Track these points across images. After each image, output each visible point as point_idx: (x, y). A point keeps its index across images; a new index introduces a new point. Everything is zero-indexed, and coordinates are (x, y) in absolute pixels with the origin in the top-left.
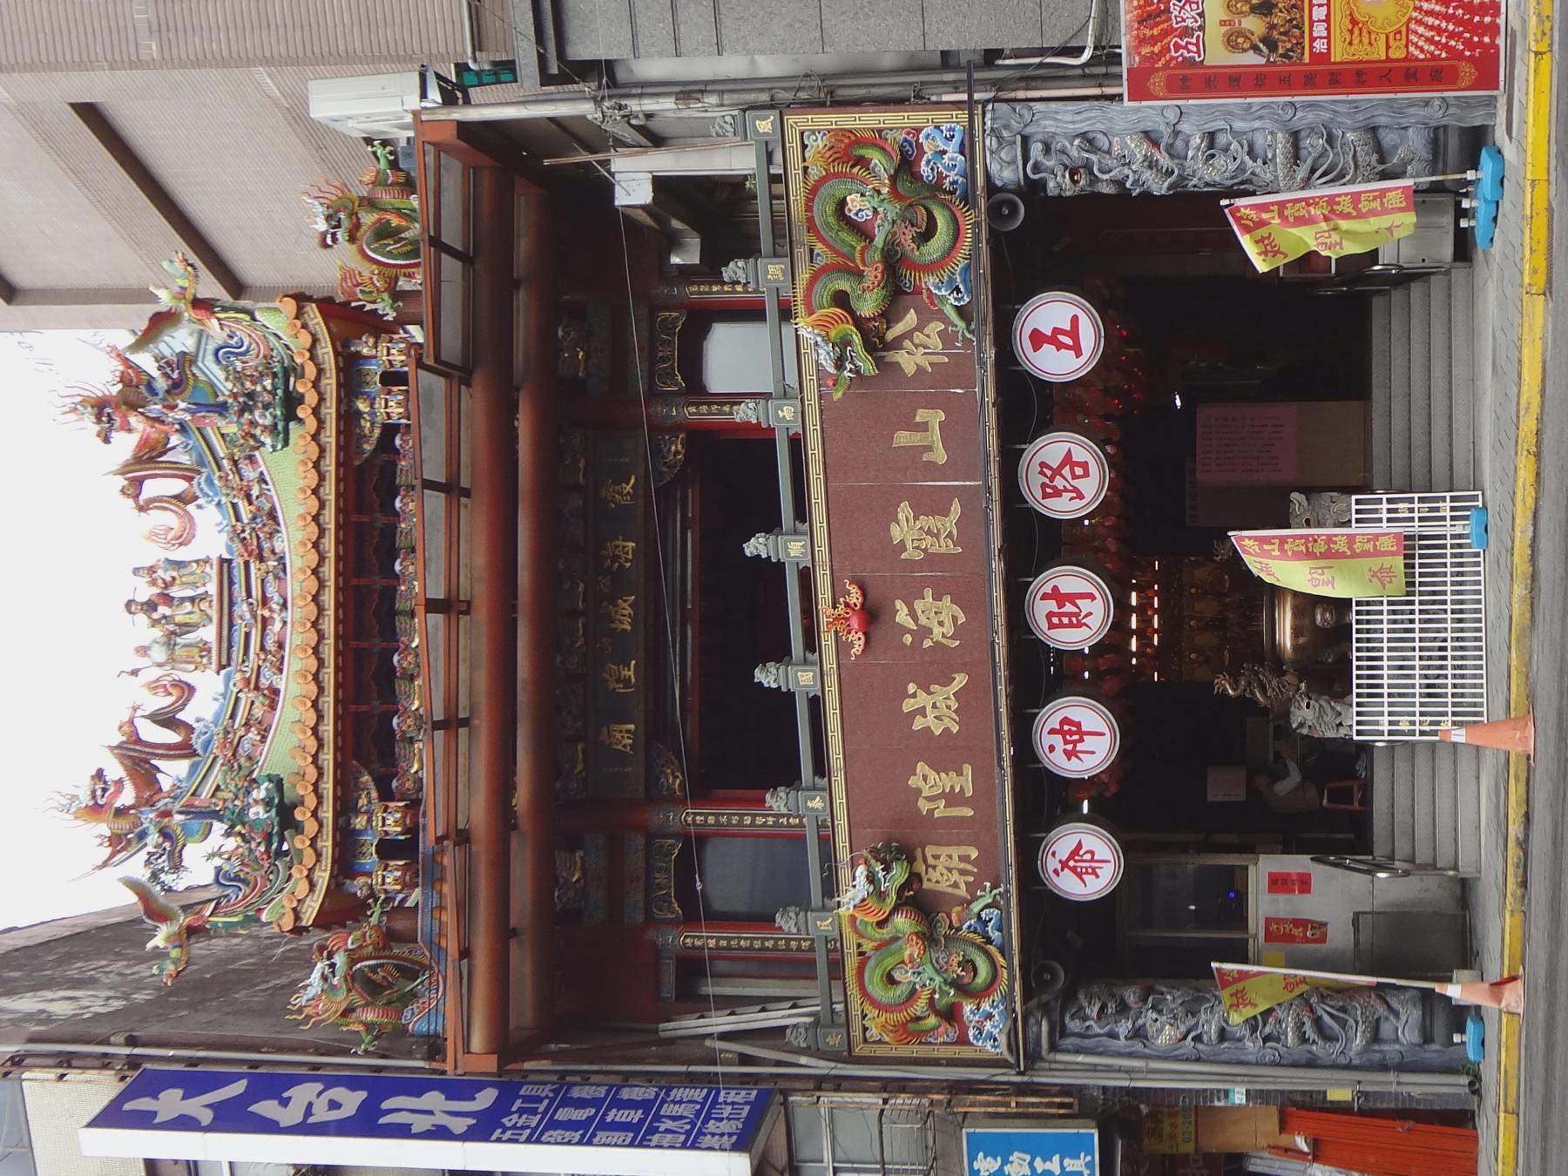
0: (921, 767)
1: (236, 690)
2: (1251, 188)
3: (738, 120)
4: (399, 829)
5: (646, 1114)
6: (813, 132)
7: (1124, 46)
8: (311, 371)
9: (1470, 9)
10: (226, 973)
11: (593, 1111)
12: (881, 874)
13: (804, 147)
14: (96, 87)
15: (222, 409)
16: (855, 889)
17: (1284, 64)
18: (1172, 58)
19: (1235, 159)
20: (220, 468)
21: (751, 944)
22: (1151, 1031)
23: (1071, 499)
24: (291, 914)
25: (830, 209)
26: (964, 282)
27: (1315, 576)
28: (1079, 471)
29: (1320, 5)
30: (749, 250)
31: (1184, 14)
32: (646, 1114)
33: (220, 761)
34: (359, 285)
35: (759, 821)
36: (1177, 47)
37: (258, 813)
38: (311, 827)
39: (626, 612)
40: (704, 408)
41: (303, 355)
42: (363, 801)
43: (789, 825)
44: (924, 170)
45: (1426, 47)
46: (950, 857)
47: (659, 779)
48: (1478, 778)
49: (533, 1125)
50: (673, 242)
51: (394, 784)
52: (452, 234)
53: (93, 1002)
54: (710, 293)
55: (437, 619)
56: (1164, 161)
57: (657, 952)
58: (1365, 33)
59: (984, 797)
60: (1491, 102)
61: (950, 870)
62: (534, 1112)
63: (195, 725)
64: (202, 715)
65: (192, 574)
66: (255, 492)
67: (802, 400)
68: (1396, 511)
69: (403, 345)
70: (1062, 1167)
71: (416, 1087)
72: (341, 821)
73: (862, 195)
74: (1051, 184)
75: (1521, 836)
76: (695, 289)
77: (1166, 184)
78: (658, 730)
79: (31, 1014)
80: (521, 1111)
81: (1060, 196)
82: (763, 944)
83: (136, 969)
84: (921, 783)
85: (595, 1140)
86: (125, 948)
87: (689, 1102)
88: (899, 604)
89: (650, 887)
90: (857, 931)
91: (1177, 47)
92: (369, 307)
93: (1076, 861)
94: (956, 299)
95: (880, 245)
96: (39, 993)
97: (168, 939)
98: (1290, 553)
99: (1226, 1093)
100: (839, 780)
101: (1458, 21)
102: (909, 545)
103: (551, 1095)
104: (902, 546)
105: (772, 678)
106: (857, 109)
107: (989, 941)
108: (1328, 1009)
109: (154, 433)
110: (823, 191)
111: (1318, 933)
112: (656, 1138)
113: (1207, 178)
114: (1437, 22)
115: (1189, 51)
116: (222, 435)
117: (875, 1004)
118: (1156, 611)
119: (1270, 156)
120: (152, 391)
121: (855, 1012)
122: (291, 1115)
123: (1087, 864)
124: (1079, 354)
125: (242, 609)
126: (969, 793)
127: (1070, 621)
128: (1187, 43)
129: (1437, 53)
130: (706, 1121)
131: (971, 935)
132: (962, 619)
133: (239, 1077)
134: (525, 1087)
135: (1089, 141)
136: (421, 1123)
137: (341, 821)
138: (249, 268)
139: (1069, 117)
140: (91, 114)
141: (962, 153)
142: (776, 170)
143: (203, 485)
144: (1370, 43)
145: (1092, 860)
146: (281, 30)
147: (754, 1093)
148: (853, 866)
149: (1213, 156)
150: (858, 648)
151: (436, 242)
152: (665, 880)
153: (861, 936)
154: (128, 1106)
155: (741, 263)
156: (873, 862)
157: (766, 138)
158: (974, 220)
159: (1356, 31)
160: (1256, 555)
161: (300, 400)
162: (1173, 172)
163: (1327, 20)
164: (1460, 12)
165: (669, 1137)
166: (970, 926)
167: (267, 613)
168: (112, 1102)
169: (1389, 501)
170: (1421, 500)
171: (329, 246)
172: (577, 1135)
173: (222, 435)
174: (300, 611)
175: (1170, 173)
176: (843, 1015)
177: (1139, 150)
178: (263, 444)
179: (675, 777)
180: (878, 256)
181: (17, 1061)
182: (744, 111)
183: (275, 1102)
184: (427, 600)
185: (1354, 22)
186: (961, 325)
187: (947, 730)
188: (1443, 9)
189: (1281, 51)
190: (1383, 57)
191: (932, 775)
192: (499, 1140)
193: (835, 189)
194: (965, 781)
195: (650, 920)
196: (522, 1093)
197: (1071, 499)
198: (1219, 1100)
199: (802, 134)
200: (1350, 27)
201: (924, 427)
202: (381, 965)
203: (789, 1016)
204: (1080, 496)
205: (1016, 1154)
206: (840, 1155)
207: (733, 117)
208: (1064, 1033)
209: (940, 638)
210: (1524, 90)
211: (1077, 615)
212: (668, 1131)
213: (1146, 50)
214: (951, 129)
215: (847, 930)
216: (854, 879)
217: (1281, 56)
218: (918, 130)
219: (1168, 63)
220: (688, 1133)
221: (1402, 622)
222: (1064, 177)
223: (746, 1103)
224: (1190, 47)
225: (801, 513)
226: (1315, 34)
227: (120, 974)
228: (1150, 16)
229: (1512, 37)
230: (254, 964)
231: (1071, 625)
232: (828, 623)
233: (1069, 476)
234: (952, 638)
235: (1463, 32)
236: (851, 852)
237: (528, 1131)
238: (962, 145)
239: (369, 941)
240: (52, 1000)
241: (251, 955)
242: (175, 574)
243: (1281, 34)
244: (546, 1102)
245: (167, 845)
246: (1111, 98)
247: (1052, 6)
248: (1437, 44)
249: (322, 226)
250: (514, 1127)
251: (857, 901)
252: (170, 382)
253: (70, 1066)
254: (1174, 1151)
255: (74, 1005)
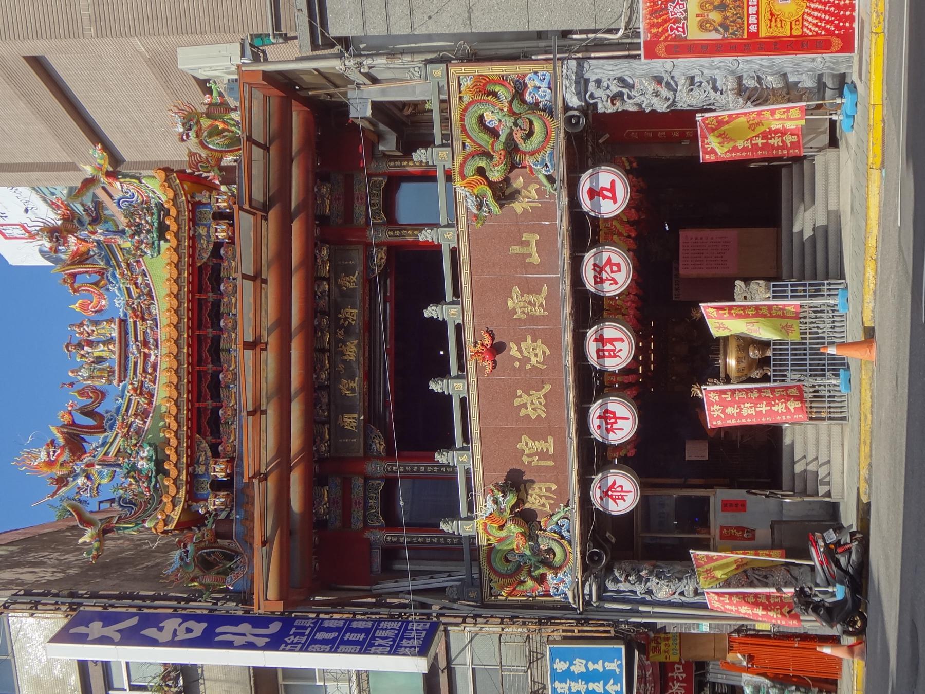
0: (524, 438)
1: (128, 395)
2: (714, 108)
3: (423, 69)
4: (223, 474)
5: (367, 636)
6: (465, 76)
7: (641, 27)
8: (173, 212)
9: (837, 7)
10: (118, 559)
11: (337, 634)
12: (501, 499)
13: (460, 85)
14: (37, 48)
15: (123, 233)
16: (485, 507)
17: (732, 39)
18: (669, 35)
19: (705, 92)
20: (120, 267)
21: (425, 540)
22: (654, 591)
23: (611, 284)
24: (162, 522)
25: (474, 120)
26: (551, 161)
27: (749, 327)
28: (615, 268)
29: (753, 6)
30: (428, 142)
31: (676, 11)
32: (367, 636)
33: (120, 436)
34: (200, 162)
35: (429, 469)
36: (672, 29)
37: (143, 465)
38: (174, 473)
39: (352, 350)
40: (397, 233)
41: (169, 203)
42: (202, 459)
43: (446, 472)
44: (528, 98)
45: (813, 29)
46: (540, 489)
47: (371, 445)
48: (843, 444)
49: (303, 642)
50: (380, 137)
51: (220, 448)
52: (258, 136)
53: (46, 574)
54: (401, 166)
55: (249, 353)
56: (664, 92)
57: (369, 544)
58: (778, 20)
59: (561, 454)
60: (850, 60)
61: (540, 496)
62: (303, 635)
63: (105, 415)
64: (109, 409)
65: (103, 328)
66: (140, 281)
67: (458, 228)
68: (796, 291)
69: (225, 197)
70: (604, 668)
71: (235, 621)
72: (190, 469)
73: (493, 112)
74: (600, 106)
75: (867, 476)
76: (392, 164)
77: (666, 106)
78: (373, 418)
79: (12, 581)
80: (295, 634)
81: (605, 113)
82: (431, 540)
83: (66, 556)
84: (524, 447)
85: (339, 650)
86: (58, 545)
87: (391, 629)
88: (512, 345)
89: (366, 508)
90: (487, 532)
91: (672, 29)
92: (205, 175)
93: (612, 492)
94: (546, 171)
95: (503, 141)
96: (14, 570)
97: (92, 537)
98: (734, 315)
99: (698, 625)
100: (477, 445)
101: (832, 14)
102: (518, 310)
103: (312, 625)
104: (514, 311)
105: (439, 387)
106: (490, 63)
107: (563, 538)
108: (757, 577)
109: (83, 248)
110: (470, 110)
111: (750, 535)
112: (373, 649)
113: (689, 102)
114: (819, 15)
115: (679, 31)
116: (121, 249)
117: (497, 573)
118: (653, 363)
119: (724, 90)
120: (81, 222)
121: (485, 579)
122: (166, 636)
123: (619, 494)
124: (615, 202)
125: (133, 349)
126: (552, 450)
127: (610, 354)
128: (678, 27)
129: (819, 32)
130: (401, 640)
131: (553, 534)
132: (548, 352)
133: (133, 615)
134: (297, 621)
135: (621, 80)
136: (238, 640)
137: (190, 469)
138: (127, 154)
139: (610, 68)
140: (39, 64)
141: (550, 88)
142: (445, 97)
143: (110, 278)
144: (781, 27)
145: (622, 491)
146: (164, 21)
147: (428, 624)
148: (485, 496)
149: (692, 90)
150: (488, 370)
151: (249, 139)
152: (375, 503)
153: (489, 534)
154: (72, 631)
155: (423, 151)
156: (496, 491)
157: (438, 80)
158: (558, 126)
159: (774, 20)
160: (716, 318)
161: (167, 228)
162: (669, 99)
163: (757, 14)
164: (832, 9)
165: (381, 648)
166: (552, 529)
167: (146, 351)
168: (63, 628)
169: (792, 286)
170: (810, 285)
171: (184, 141)
172: (328, 647)
173: (121, 249)
174: (165, 348)
175: (667, 99)
176: (479, 580)
177: (651, 87)
178: (146, 253)
179: (381, 445)
180: (502, 147)
181: (5, 606)
182: (426, 64)
183: (155, 629)
184: (244, 342)
185: (772, 15)
186: (549, 186)
187: (539, 416)
188: (823, 7)
189: (731, 31)
190: (789, 35)
191: (530, 443)
192: (284, 650)
193: (478, 109)
194: (549, 446)
195: (366, 526)
196: (295, 624)
197: (611, 284)
198: (694, 629)
199: (459, 78)
200: (770, 17)
201: (527, 243)
202: (213, 552)
203: (447, 581)
204: (616, 283)
205: (577, 660)
206: (476, 661)
207: (420, 68)
208: (606, 590)
209: (535, 363)
210: (868, 54)
211: (613, 351)
212: (380, 645)
213: (654, 31)
214: (543, 75)
215: (481, 531)
216: (486, 502)
217: (731, 34)
218: (525, 76)
219: (667, 38)
220: (391, 646)
221: (800, 355)
222: (607, 101)
223: (424, 630)
224: (680, 29)
225: (457, 292)
226: (750, 22)
227: (57, 559)
228: (656, 11)
229: (862, 23)
230: (132, 554)
231: (610, 356)
232: (472, 355)
233: (609, 272)
234: (542, 363)
235: (834, 20)
236: (484, 486)
237: (300, 645)
238: (549, 83)
239: (206, 538)
240: (22, 573)
241: (130, 550)
242: (94, 328)
243: (731, 22)
244: (309, 629)
245: (89, 483)
246: (634, 57)
247: (601, 5)
248: (819, 27)
249: (181, 130)
250: (292, 643)
251: (488, 514)
252: (91, 218)
253: (37, 609)
254: (667, 660)
255: (35, 576)
